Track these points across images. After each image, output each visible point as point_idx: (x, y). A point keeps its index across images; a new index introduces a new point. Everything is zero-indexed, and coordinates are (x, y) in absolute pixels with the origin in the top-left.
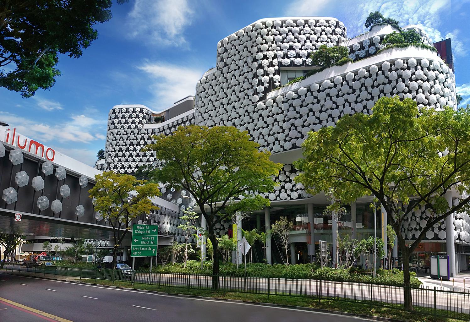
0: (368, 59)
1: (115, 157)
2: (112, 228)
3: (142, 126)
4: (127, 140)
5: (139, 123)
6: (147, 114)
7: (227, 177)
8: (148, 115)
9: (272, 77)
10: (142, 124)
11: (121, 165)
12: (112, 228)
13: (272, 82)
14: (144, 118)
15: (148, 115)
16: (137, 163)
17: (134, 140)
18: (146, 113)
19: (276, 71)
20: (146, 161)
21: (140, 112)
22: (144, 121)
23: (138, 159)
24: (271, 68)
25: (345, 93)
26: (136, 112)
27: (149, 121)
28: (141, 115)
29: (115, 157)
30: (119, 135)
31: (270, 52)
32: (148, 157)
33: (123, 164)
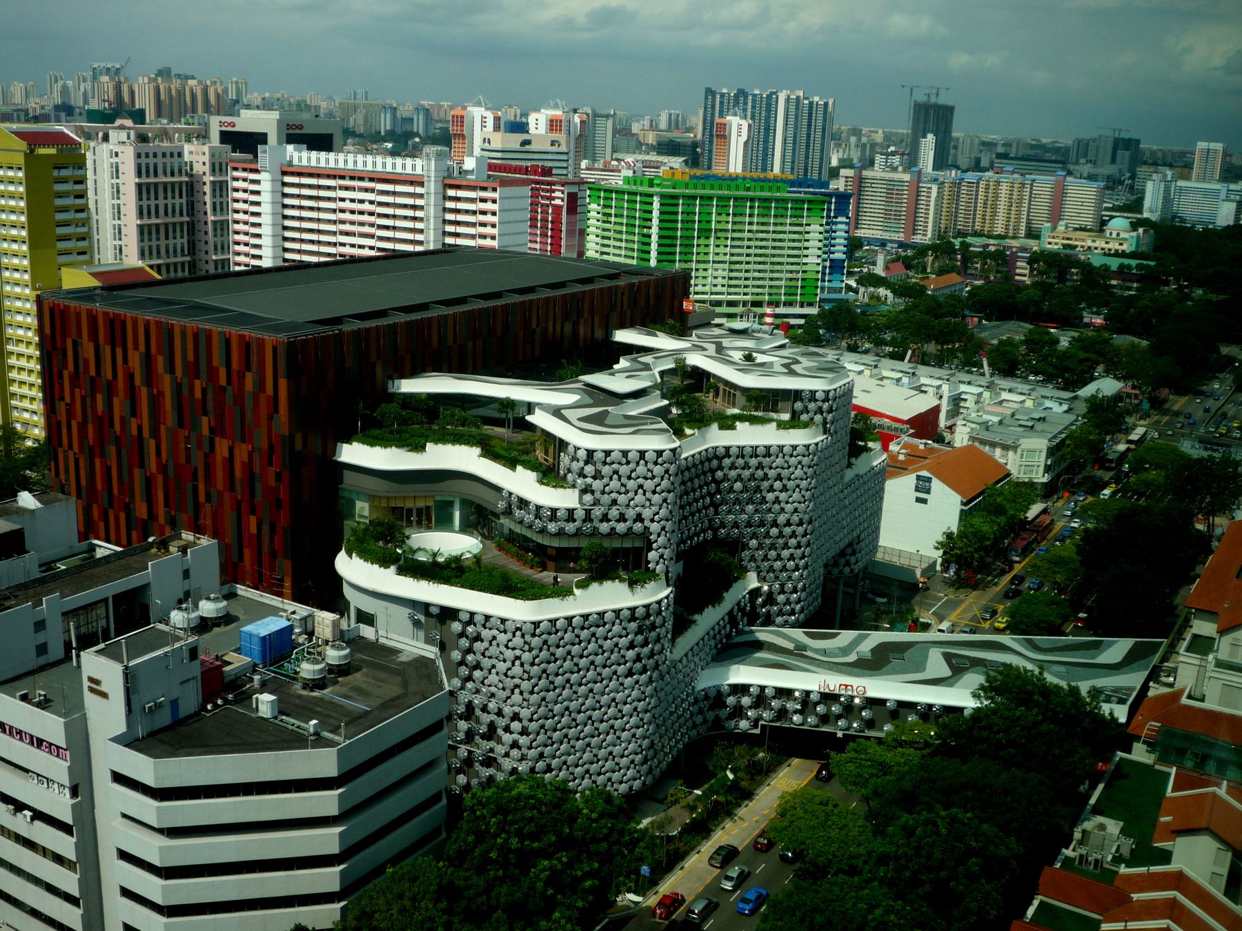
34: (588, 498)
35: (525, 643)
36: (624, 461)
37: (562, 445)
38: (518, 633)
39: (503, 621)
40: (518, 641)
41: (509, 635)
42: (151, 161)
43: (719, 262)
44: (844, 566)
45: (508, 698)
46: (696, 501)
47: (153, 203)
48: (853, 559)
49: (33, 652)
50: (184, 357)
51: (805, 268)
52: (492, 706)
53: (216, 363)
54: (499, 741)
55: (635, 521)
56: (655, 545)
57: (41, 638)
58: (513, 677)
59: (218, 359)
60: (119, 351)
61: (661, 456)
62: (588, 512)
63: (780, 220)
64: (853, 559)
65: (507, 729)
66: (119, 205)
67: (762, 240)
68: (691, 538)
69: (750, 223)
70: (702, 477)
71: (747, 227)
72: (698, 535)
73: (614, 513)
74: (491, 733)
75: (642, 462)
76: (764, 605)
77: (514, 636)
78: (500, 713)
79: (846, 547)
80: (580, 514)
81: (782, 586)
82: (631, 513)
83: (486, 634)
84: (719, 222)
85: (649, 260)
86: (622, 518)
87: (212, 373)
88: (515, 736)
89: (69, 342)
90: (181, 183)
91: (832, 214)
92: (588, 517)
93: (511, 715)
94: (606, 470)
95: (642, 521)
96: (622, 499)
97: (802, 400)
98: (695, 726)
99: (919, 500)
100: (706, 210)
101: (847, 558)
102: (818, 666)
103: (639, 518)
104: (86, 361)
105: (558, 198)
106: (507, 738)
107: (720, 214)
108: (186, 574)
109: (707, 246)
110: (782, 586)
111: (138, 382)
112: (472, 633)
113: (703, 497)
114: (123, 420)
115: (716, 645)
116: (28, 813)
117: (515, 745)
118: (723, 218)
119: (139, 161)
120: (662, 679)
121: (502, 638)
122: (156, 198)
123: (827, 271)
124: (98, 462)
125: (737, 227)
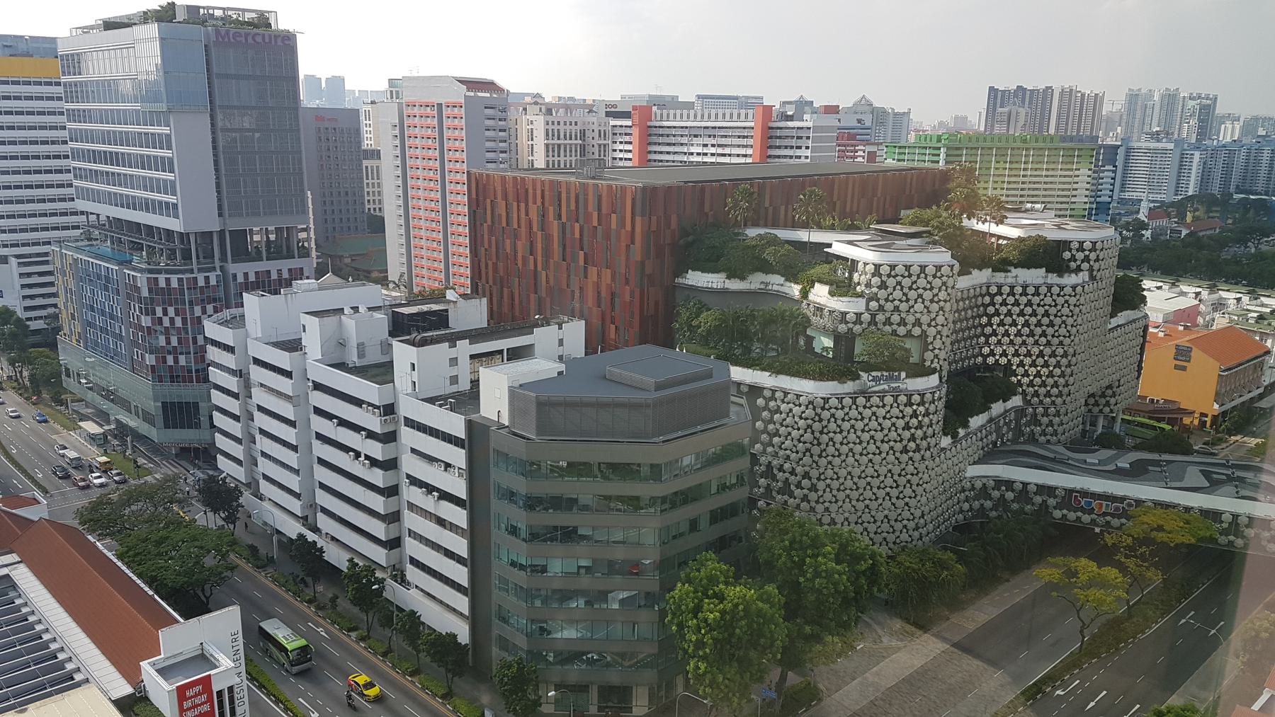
34: (874, 304)
35: (816, 414)
36: (907, 274)
37: (854, 263)
38: (808, 454)
39: (798, 396)
40: (810, 413)
41: (803, 408)
42: (556, 127)
43: (999, 175)
44: (1104, 406)
45: (801, 459)
46: (969, 329)
47: (556, 159)
48: (1113, 401)
49: (448, 382)
50: (568, 206)
51: (1073, 206)
52: (787, 466)
53: (590, 209)
54: (791, 495)
55: (914, 325)
56: (930, 347)
57: (454, 371)
58: (805, 443)
59: (592, 207)
60: (523, 205)
61: (940, 271)
62: (873, 316)
63: (1052, 166)
64: (1113, 401)
65: (799, 486)
66: (532, 145)
67: (1034, 183)
68: (963, 360)
69: (1025, 169)
70: (975, 310)
71: (1022, 173)
72: (969, 359)
73: (896, 318)
74: (786, 489)
75: (923, 275)
76: (1028, 424)
77: (806, 432)
78: (793, 472)
79: (1107, 388)
80: (866, 317)
81: (1046, 409)
82: (911, 319)
83: (783, 407)
84: (997, 169)
85: (938, 162)
86: (903, 323)
87: (588, 217)
88: (805, 491)
89: (488, 201)
90: (576, 145)
91: (1100, 164)
92: (873, 322)
93: (803, 474)
94: (891, 282)
95: (920, 325)
96: (904, 307)
97: (1070, 250)
98: (961, 511)
99: (1176, 367)
100: (986, 158)
101: (1108, 399)
102: (1078, 471)
103: (918, 323)
104: (500, 215)
105: (860, 156)
106: (798, 492)
107: (998, 162)
108: (561, 342)
109: (986, 188)
110: (1046, 409)
111: (535, 229)
112: (773, 407)
113: (975, 327)
114: (524, 259)
115: (983, 448)
116: (435, 494)
117: (805, 498)
118: (1001, 165)
119: (547, 127)
120: (933, 460)
121: (796, 410)
122: (559, 156)
123: (1094, 212)
124: (505, 290)
125: (1013, 172)
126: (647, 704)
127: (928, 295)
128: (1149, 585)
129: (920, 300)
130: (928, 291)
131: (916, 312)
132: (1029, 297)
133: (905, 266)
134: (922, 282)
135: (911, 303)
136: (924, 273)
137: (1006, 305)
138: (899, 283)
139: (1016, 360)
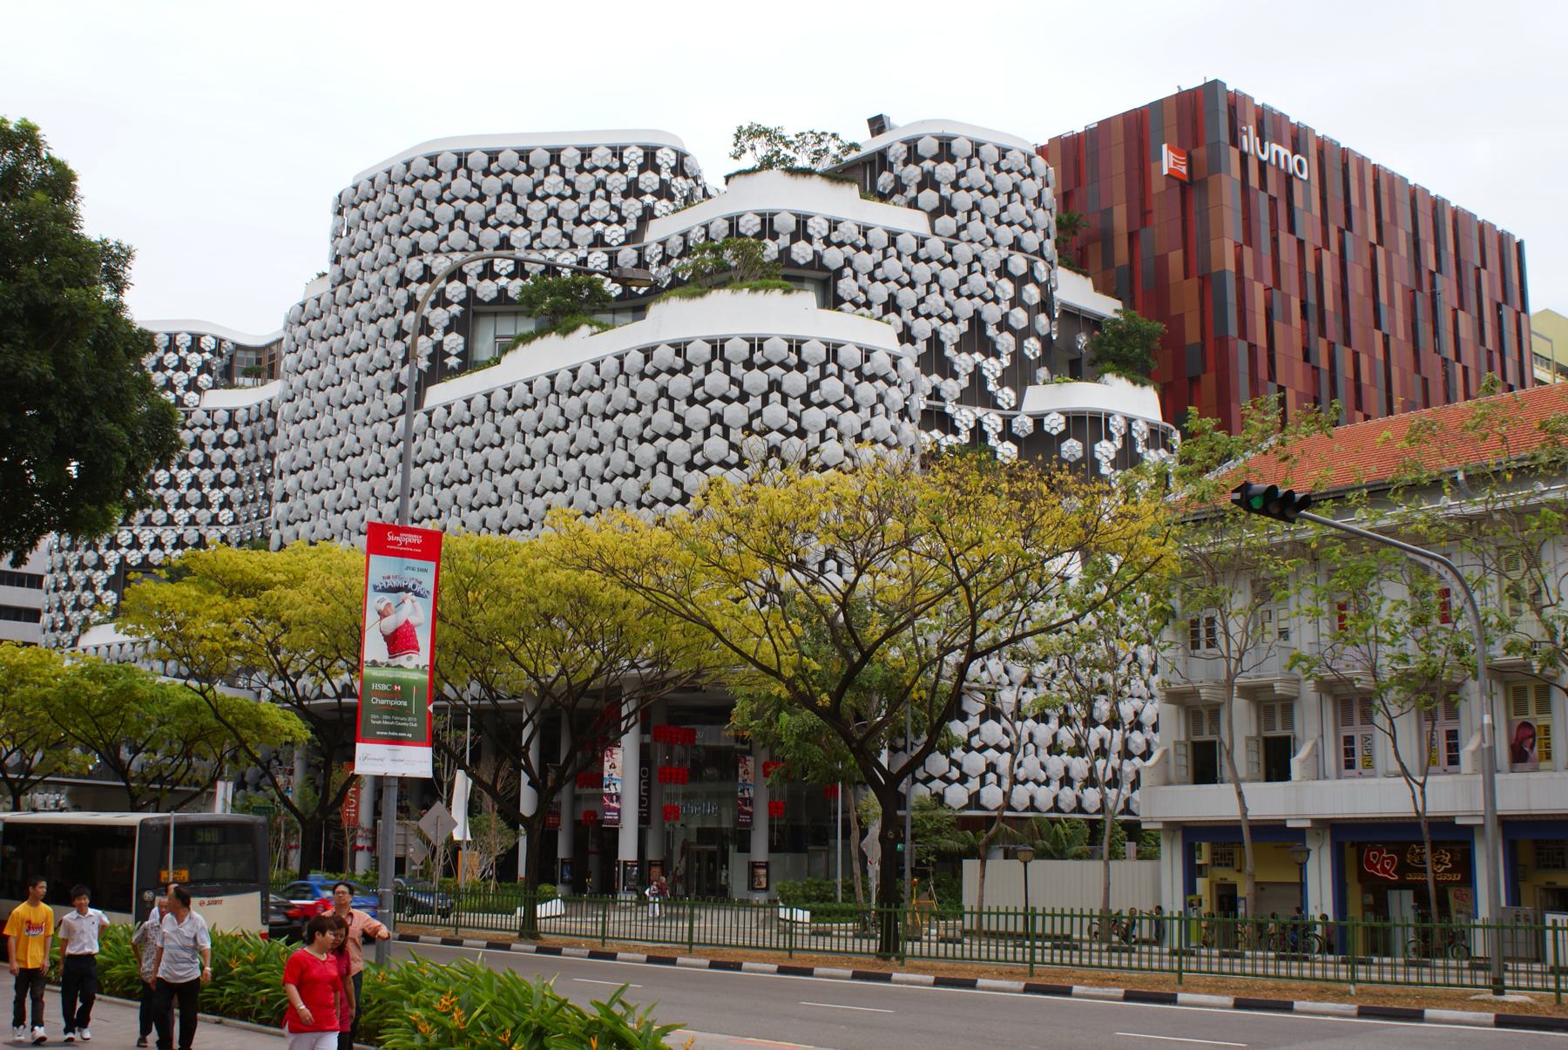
0: (1080, 129)
1: (625, 195)
2: (123, 784)
3: (197, 397)
4: (484, 224)
5: (187, 388)
6: (217, 352)
7: (890, 520)
8: (221, 355)
9: (585, 255)
10: (199, 391)
11: (130, 535)
12: (123, 784)
13: (438, 353)
14: (205, 368)
15: (221, 355)
16: (180, 531)
17: (561, 197)
18: (212, 352)
19: (453, 319)
20: (209, 524)
21: (190, 350)
22: (205, 380)
23: (182, 516)
24: (487, 282)
25: (716, 394)
26: (176, 350)
27: (226, 378)
28: (195, 359)
29: (625, 195)
30: (450, 203)
31: (441, 258)
32: (215, 510)
33: (136, 532)
126: (1101, 863)
127: (568, 209)
128: (464, 751)
129: (459, 223)
130: (475, 204)
131: (546, 248)
132: (928, 165)
133: (613, 148)
134: (461, 185)
135: (536, 228)
136: (559, 163)
137: (639, 194)
138: (775, 385)
139: (439, 317)
